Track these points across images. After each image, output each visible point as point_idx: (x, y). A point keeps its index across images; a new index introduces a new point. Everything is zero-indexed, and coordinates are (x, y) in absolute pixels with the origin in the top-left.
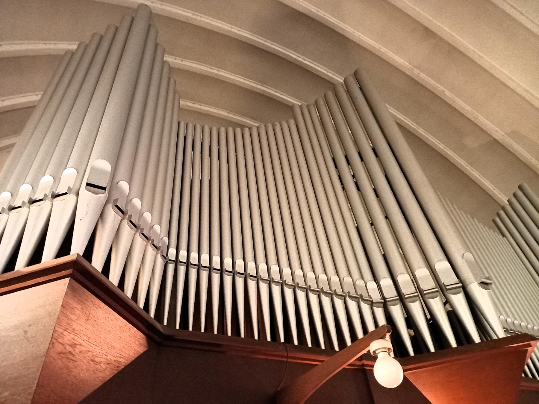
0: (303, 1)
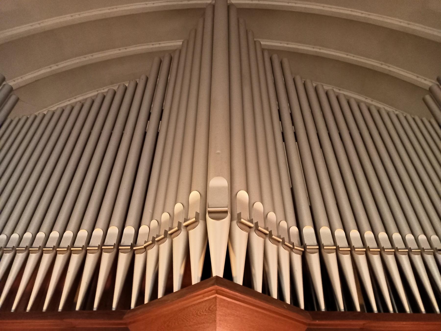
0: (1, 86)
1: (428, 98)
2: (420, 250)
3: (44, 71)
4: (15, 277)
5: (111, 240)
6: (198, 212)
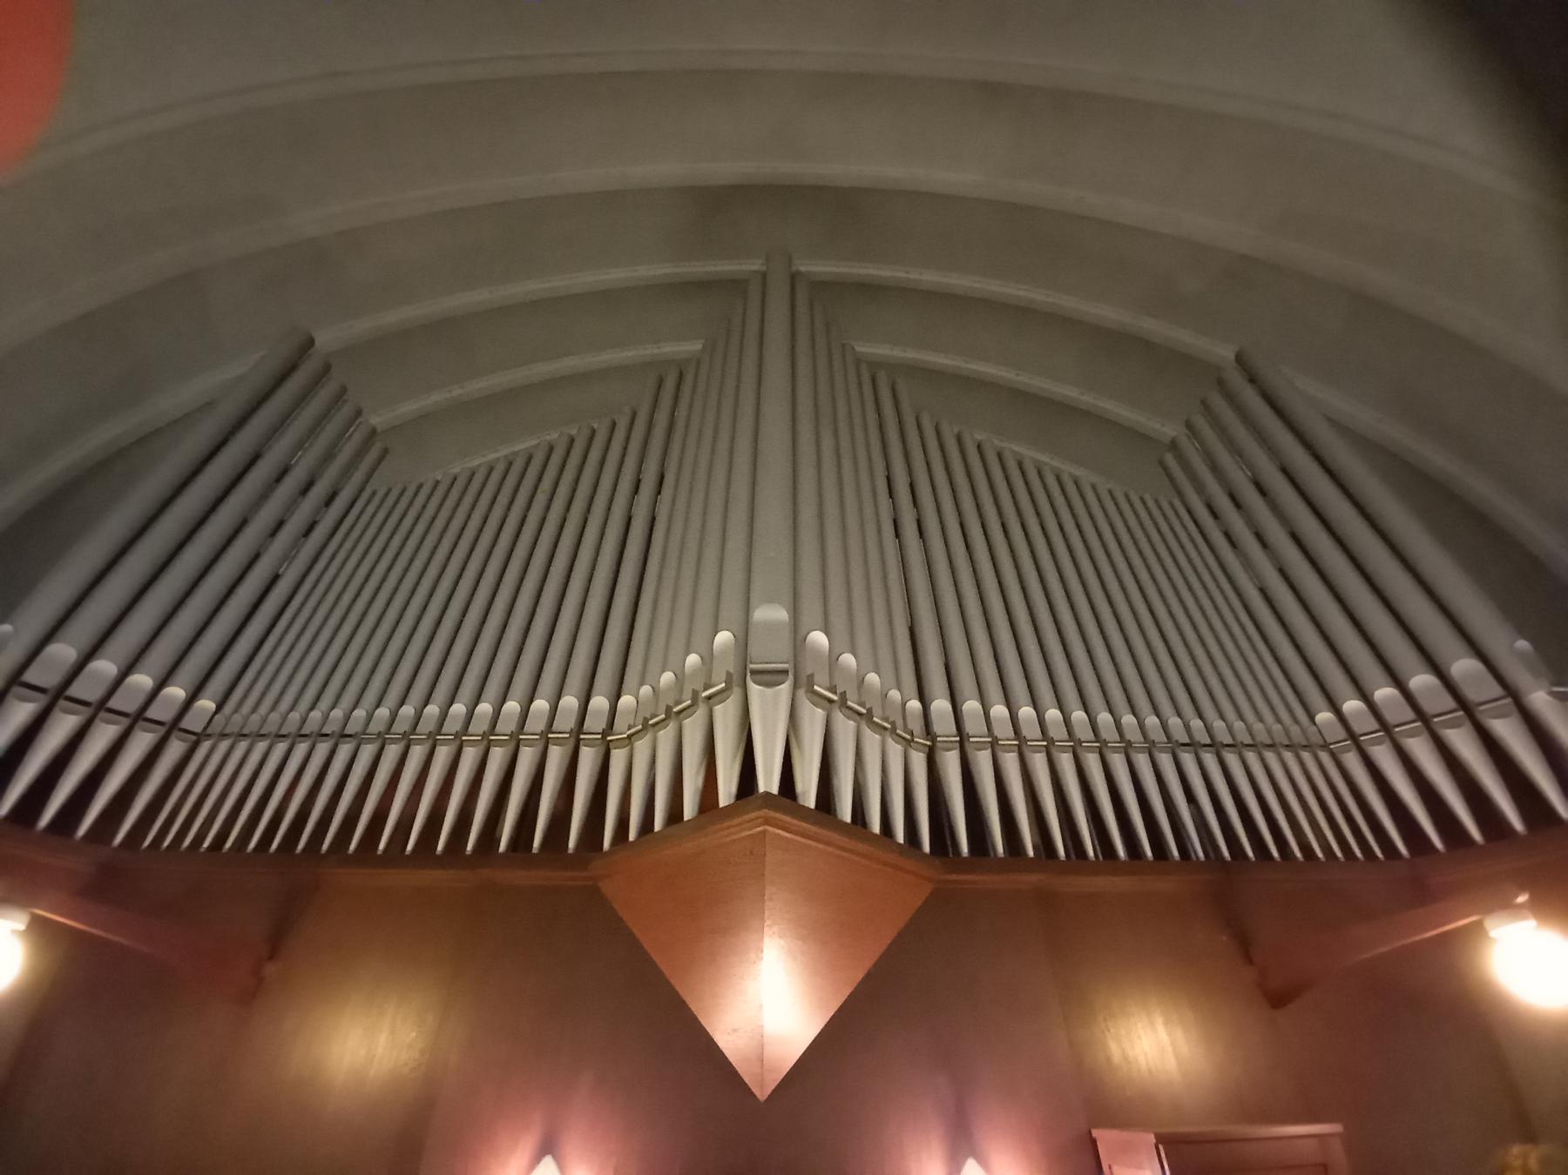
1: (1170, 459)
2: (1147, 745)
3: (436, 398)
4: (383, 789)
5: (566, 722)
6: (731, 671)
